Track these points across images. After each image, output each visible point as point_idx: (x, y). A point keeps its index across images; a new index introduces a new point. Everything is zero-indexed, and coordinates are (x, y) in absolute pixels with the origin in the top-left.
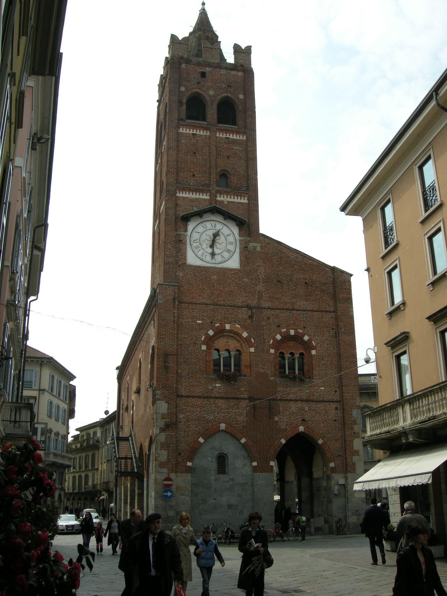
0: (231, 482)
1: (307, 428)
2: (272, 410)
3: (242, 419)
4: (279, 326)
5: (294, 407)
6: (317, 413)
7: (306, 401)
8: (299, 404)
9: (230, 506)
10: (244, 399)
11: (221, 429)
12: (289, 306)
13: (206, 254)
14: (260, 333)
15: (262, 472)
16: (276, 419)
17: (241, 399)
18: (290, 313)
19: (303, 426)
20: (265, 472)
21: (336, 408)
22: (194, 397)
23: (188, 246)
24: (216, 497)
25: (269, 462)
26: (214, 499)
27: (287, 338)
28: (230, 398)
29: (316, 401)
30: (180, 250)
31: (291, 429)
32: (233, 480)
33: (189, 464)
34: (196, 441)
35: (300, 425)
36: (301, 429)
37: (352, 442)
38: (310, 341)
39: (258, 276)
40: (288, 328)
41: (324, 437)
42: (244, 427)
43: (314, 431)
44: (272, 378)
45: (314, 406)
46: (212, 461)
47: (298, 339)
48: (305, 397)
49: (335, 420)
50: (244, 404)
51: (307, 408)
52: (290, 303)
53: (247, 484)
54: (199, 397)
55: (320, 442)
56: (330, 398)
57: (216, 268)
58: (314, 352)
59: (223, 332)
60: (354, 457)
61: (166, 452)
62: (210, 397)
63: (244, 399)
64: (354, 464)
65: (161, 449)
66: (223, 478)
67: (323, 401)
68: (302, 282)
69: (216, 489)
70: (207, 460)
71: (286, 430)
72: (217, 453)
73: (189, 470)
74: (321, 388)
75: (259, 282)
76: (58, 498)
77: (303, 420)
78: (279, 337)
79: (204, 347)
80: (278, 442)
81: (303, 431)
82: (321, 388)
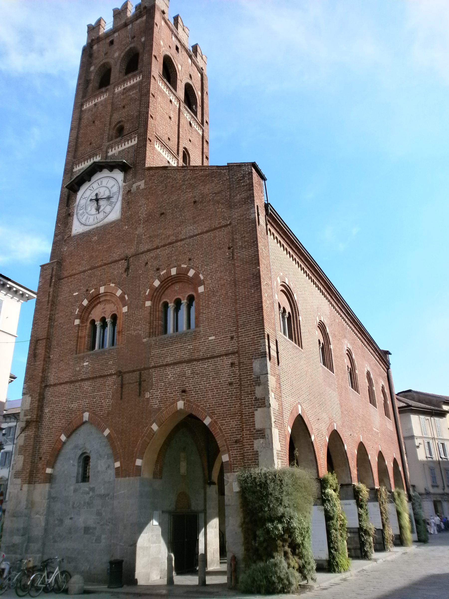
0: (91, 494)
1: (188, 402)
2: (142, 385)
3: (107, 403)
4: (158, 269)
5: (171, 373)
6: (202, 377)
7: (189, 361)
8: (178, 369)
9: (87, 530)
10: (111, 375)
11: (84, 420)
12: (173, 238)
13: (95, 216)
14: (135, 285)
15: (125, 477)
16: (147, 395)
17: (108, 375)
18: (173, 247)
19: (183, 400)
20: (129, 476)
21: (232, 364)
22: (61, 384)
23: (75, 216)
24: (72, 516)
25: (135, 461)
26: (71, 519)
27: (168, 282)
28: (96, 377)
29: (202, 359)
30: (68, 224)
31: (167, 408)
32: (92, 489)
33: (49, 471)
34: (57, 440)
35: (178, 400)
36: (180, 405)
37: (253, 416)
38: (196, 275)
39: (139, 217)
40: (169, 268)
41: (213, 413)
42: (108, 414)
43: (199, 406)
44: (145, 340)
45: (199, 366)
46: (73, 465)
47: (181, 277)
48: (186, 357)
49: (231, 384)
50: (110, 381)
51: (188, 372)
52: (173, 235)
53: (108, 495)
54: (66, 383)
55: (207, 421)
56: (223, 350)
57: (97, 228)
58: (201, 289)
59: (99, 298)
60: (256, 442)
61: (23, 457)
62: (77, 381)
63: (111, 375)
64: (256, 454)
65: (19, 455)
66: (85, 487)
67: (212, 357)
68: (190, 203)
69: (74, 503)
70: (68, 466)
71: (159, 409)
72: (80, 452)
73: (50, 479)
74: (210, 338)
75: (140, 224)
76: (409, 490)
77: (184, 391)
78: (157, 283)
79: (77, 322)
80: (148, 429)
81: (183, 408)
82: (210, 338)
